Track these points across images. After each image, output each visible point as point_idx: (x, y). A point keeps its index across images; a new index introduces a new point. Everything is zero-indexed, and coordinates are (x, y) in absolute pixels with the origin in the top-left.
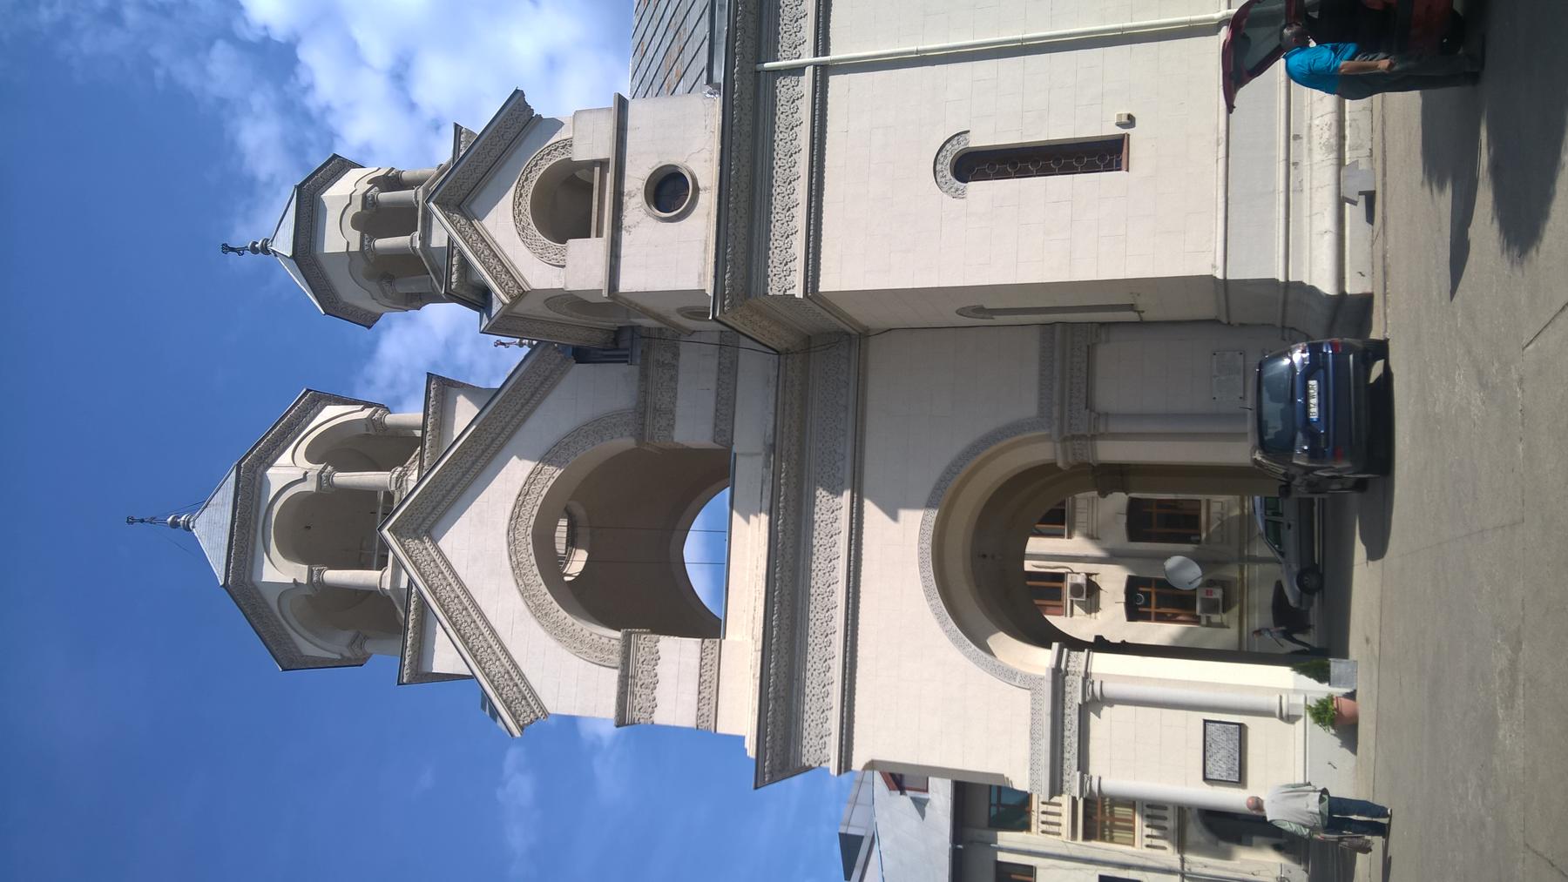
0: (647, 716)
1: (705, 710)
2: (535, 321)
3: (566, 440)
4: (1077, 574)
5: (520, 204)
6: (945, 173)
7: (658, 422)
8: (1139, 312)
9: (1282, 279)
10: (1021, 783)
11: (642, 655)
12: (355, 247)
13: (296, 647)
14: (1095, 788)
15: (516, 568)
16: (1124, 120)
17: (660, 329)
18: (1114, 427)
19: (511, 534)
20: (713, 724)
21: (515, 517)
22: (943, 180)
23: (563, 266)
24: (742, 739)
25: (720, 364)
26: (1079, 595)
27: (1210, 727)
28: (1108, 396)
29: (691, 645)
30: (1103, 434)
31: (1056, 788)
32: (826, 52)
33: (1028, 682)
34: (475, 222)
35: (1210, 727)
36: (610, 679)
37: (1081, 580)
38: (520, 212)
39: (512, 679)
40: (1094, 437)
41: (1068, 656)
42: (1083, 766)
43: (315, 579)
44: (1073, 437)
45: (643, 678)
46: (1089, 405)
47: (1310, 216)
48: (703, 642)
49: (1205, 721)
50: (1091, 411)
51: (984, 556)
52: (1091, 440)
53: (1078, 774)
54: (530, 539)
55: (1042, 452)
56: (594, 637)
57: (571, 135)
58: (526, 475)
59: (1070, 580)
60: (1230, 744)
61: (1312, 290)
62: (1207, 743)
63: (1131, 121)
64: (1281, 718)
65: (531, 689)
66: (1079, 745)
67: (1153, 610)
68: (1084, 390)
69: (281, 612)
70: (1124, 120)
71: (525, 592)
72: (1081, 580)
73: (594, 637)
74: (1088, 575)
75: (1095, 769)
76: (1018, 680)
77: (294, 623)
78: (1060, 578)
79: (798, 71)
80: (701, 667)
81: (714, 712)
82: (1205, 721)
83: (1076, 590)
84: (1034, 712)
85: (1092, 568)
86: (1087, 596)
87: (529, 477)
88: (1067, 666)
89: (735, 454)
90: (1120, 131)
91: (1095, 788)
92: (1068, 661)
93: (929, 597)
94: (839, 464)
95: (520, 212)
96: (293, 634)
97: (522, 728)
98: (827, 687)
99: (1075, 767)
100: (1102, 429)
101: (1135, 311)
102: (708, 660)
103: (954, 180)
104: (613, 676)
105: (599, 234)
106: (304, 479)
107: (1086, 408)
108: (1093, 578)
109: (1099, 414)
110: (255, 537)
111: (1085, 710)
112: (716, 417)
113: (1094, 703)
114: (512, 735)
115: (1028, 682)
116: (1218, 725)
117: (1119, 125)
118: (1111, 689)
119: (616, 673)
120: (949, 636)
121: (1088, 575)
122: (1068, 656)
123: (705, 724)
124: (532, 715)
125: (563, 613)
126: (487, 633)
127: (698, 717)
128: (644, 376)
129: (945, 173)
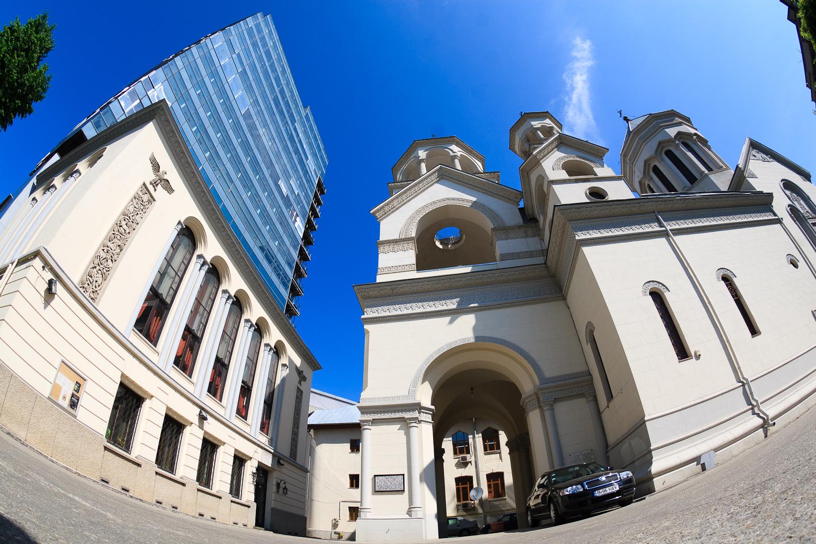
0: (382, 251)
2: (529, 185)
4: (470, 458)
8: (608, 407)
9: (652, 448)
10: (364, 395)
11: (406, 245)
14: (365, 427)
15: (434, 203)
16: (698, 354)
17: (540, 229)
18: (547, 414)
23: (554, 170)
25: (534, 251)
26: (462, 460)
27: (402, 477)
28: (562, 408)
29: (413, 260)
30: (543, 410)
31: (364, 410)
32: (675, 234)
33: (412, 392)
34: (556, 149)
35: (402, 477)
37: (468, 460)
39: (392, 209)
40: (540, 407)
41: (429, 414)
42: (374, 422)
44: (538, 398)
45: (396, 247)
46: (556, 400)
47: (665, 234)
48: (414, 264)
49: (403, 475)
50: (554, 401)
51: (472, 389)
52: (539, 406)
53: (371, 419)
55: (527, 384)
56: (411, 229)
59: (468, 456)
60: (395, 484)
61: (650, 463)
62: (393, 476)
63: (698, 357)
64: (410, 508)
65: (389, 215)
66: (387, 419)
67: (461, 486)
68: (562, 396)
70: (698, 354)
72: (468, 460)
73: (411, 229)
74: (471, 462)
75: (375, 429)
76: (413, 389)
78: (468, 452)
79: (661, 225)
82: (403, 475)
83: (464, 458)
84: (398, 397)
85: (473, 463)
86: (462, 463)
88: (423, 412)
90: (693, 354)
91: (365, 427)
92: (426, 413)
94: (503, 298)
98: (399, 310)
99: (374, 418)
100: (545, 409)
101: (608, 404)
104: (397, 237)
106: (454, 152)
107: (555, 399)
108: (470, 464)
109: (552, 406)
111: (402, 420)
112: (511, 254)
113: (406, 424)
115: (412, 392)
116: (402, 480)
117: (695, 353)
118: (414, 431)
119: (398, 238)
121: (471, 462)
124: (379, 217)
125: (419, 219)
127: (382, 268)
128: (519, 227)
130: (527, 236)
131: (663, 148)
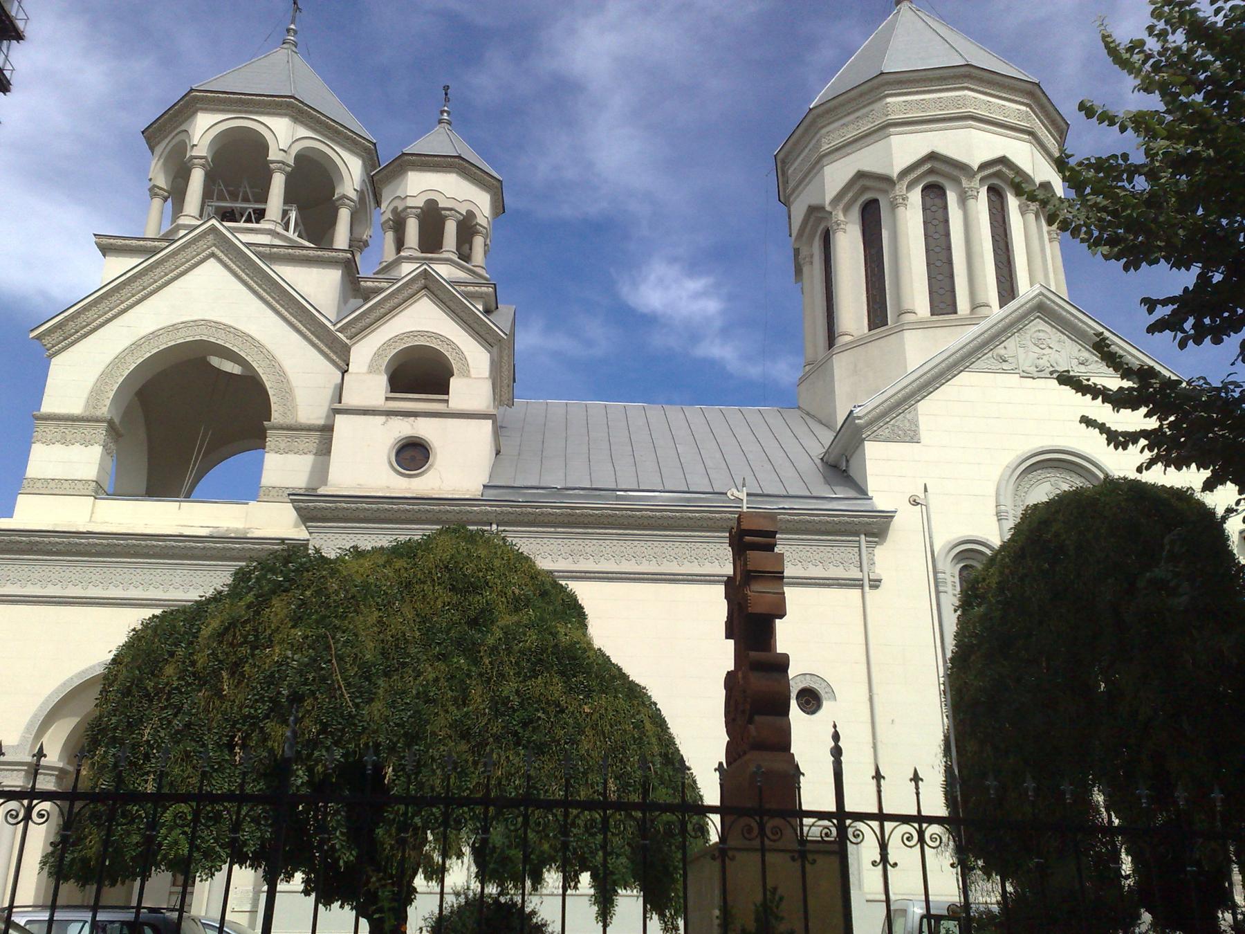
1: (39, 484)
3: (276, 365)
5: (408, 337)
6: (804, 682)
7: (283, 440)
12: (410, 203)
13: (159, 143)
15: (175, 327)
19: (203, 322)
20: (25, 492)
21: (218, 326)
22: (798, 681)
24: (10, 515)
36: (75, 407)
38: (402, 339)
43: (196, 161)
54: (198, 338)
57: (473, 376)
58: (251, 333)
65: (73, 343)
69: (179, 132)
71: (154, 335)
77: (174, 142)
80: (73, 480)
81: (35, 492)
87: (249, 336)
89: (247, 504)
95: (402, 339)
96: (166, 141)
97: (38, 338)
102: (80, 485)
103: (799, 688)
105: (387, 399)
110: (163, 140)
114: (32, 330)
120: (67, 681)
122: (53, 775)
123: (26, 486)
127: (32, 479)
129: (804, 682)
131: (865, 189)
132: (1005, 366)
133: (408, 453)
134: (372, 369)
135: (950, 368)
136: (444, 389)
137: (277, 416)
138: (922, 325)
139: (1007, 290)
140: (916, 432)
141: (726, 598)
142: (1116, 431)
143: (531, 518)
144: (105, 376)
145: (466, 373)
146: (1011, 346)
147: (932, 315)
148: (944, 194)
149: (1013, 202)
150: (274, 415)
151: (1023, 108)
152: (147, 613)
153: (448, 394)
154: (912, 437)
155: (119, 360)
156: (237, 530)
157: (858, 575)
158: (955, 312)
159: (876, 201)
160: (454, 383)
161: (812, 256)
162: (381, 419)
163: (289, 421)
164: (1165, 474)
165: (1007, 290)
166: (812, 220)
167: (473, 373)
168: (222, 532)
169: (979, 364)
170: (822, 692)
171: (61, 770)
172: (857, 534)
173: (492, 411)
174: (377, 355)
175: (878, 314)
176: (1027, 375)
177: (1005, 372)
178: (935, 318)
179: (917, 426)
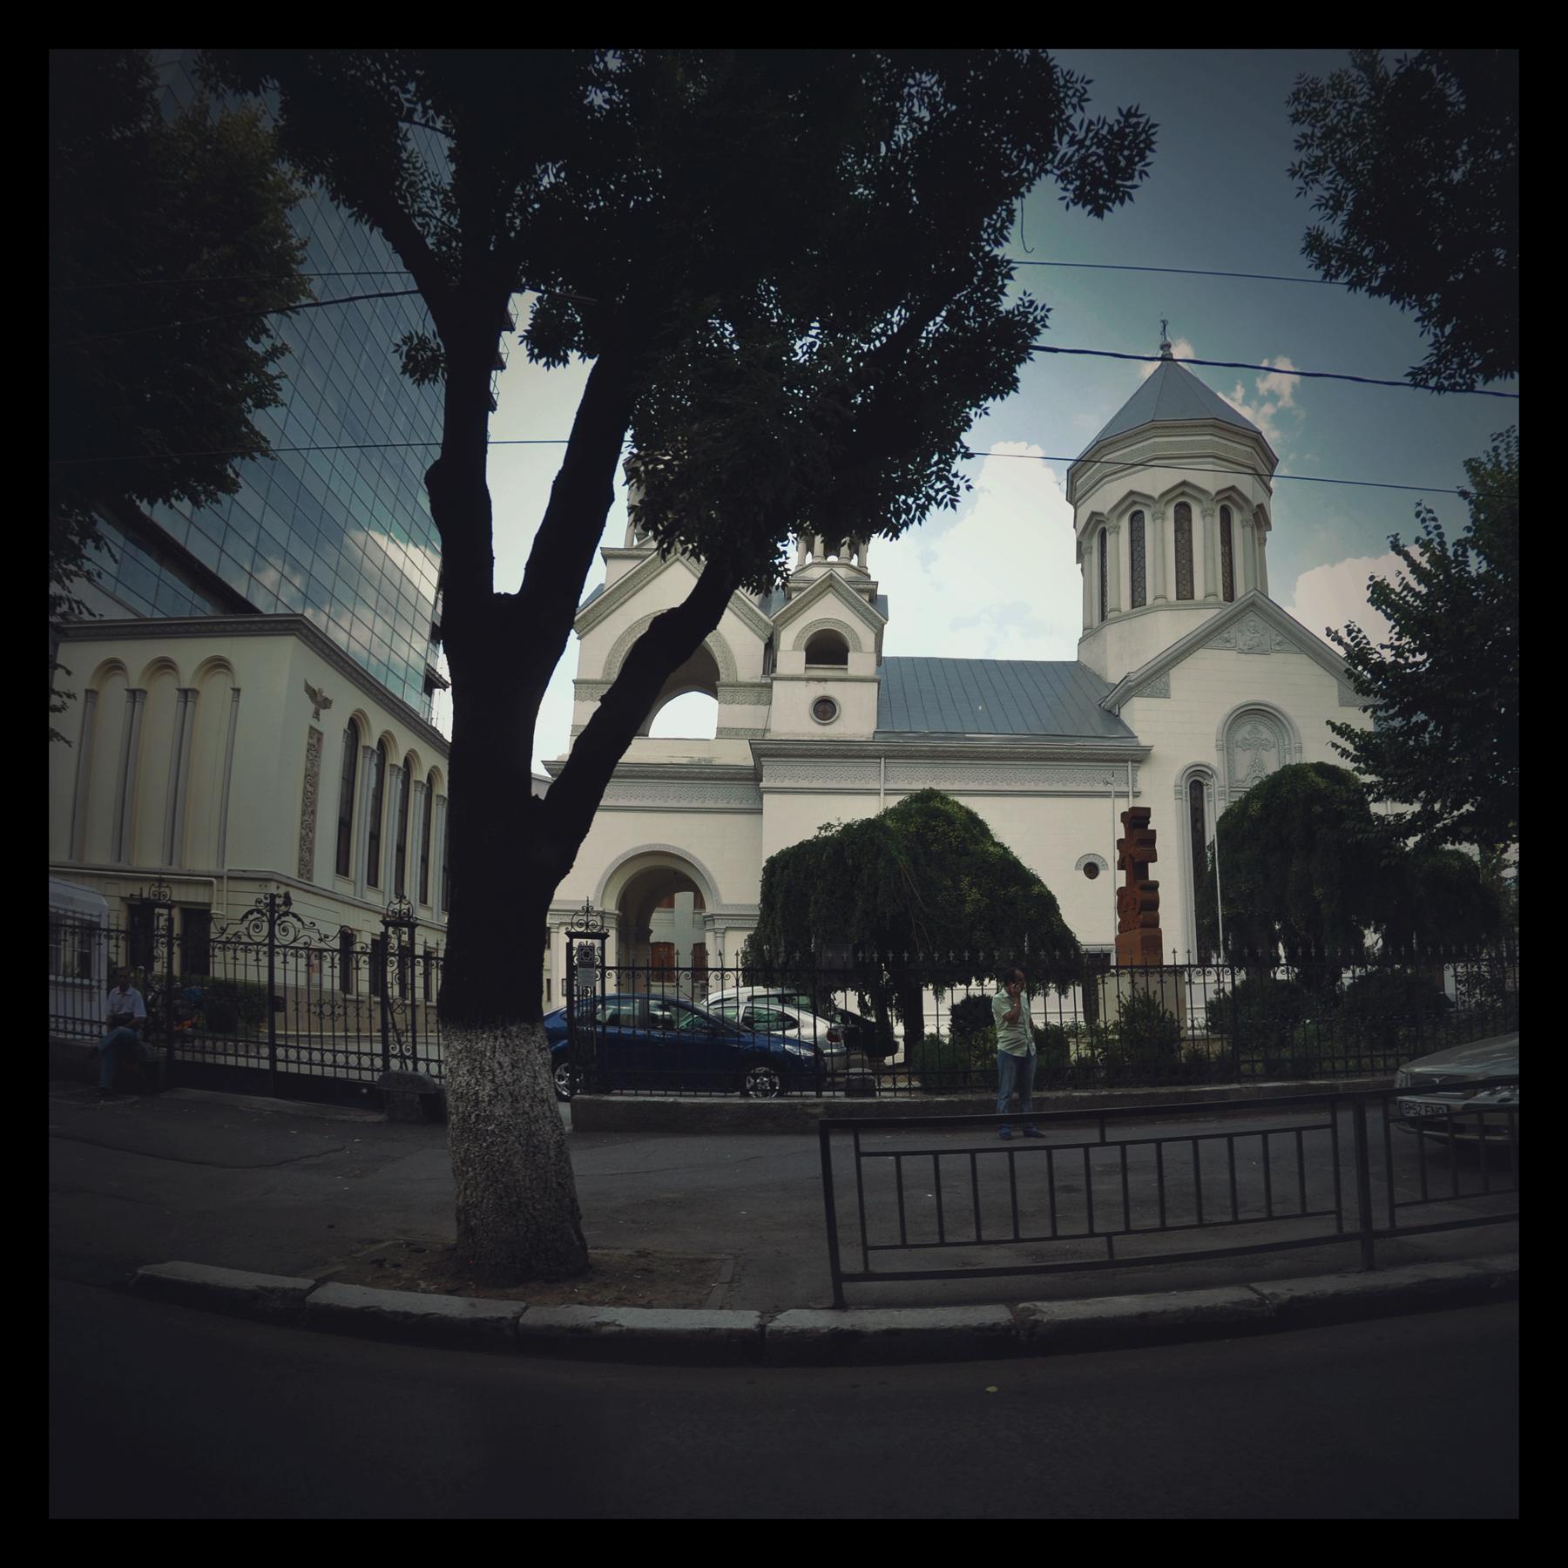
93: (633, 850)
126: (622, 600)
128: (754, 685)
130: (758, 703)
132: (1228, 645)
133: (821, 708)
134: (795, 648)
135: (1192, 646)
136: (843, 660)
137: (723, 677)
138: (1169, 607)
139: (1229, 594)
140: (1168, 691)
141: (571, 866)
142: (1408, 566)
143: (908, 753)
144: (614, 650)
145: (859, 649)
146: (1232, 632)
147: (1178, 599)
148: (1190, 511)
149: (1236, 518)
150: (722, 676)
151: (1249, 449)
152: (901, 798)
153: (846, 664)
154: (1165, 694)
155: (621, 640)
156: (705, 760)
157: (1126, 790)
158: (1193, 598)
159: (1141, 512)
160: (851, 656)
161: (1091, 548)
162: (804, 683)
163: (731, 680)
164: (1328, 722)
165: (1229, 594)
166: (1093, 523)
167: (865, 649)
168: (695, 761)
169: (1212, 643)
170: (1100, 866)
171: (618, 915)
172: (1126, 761)
173: (878, 677)
174: (798, 637)
175: (1138, 599)
176: (1242, 652)
177: (1228, 649)
178: (1180, 602)
179: (1168, 686)
